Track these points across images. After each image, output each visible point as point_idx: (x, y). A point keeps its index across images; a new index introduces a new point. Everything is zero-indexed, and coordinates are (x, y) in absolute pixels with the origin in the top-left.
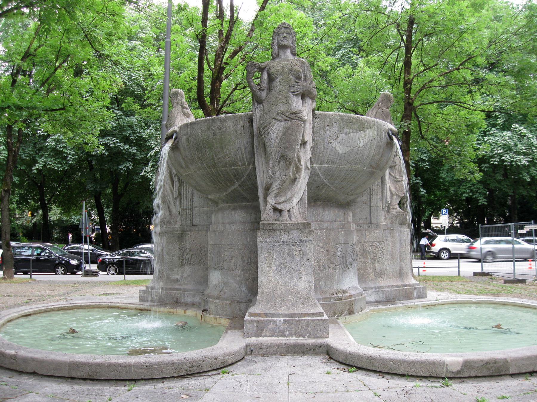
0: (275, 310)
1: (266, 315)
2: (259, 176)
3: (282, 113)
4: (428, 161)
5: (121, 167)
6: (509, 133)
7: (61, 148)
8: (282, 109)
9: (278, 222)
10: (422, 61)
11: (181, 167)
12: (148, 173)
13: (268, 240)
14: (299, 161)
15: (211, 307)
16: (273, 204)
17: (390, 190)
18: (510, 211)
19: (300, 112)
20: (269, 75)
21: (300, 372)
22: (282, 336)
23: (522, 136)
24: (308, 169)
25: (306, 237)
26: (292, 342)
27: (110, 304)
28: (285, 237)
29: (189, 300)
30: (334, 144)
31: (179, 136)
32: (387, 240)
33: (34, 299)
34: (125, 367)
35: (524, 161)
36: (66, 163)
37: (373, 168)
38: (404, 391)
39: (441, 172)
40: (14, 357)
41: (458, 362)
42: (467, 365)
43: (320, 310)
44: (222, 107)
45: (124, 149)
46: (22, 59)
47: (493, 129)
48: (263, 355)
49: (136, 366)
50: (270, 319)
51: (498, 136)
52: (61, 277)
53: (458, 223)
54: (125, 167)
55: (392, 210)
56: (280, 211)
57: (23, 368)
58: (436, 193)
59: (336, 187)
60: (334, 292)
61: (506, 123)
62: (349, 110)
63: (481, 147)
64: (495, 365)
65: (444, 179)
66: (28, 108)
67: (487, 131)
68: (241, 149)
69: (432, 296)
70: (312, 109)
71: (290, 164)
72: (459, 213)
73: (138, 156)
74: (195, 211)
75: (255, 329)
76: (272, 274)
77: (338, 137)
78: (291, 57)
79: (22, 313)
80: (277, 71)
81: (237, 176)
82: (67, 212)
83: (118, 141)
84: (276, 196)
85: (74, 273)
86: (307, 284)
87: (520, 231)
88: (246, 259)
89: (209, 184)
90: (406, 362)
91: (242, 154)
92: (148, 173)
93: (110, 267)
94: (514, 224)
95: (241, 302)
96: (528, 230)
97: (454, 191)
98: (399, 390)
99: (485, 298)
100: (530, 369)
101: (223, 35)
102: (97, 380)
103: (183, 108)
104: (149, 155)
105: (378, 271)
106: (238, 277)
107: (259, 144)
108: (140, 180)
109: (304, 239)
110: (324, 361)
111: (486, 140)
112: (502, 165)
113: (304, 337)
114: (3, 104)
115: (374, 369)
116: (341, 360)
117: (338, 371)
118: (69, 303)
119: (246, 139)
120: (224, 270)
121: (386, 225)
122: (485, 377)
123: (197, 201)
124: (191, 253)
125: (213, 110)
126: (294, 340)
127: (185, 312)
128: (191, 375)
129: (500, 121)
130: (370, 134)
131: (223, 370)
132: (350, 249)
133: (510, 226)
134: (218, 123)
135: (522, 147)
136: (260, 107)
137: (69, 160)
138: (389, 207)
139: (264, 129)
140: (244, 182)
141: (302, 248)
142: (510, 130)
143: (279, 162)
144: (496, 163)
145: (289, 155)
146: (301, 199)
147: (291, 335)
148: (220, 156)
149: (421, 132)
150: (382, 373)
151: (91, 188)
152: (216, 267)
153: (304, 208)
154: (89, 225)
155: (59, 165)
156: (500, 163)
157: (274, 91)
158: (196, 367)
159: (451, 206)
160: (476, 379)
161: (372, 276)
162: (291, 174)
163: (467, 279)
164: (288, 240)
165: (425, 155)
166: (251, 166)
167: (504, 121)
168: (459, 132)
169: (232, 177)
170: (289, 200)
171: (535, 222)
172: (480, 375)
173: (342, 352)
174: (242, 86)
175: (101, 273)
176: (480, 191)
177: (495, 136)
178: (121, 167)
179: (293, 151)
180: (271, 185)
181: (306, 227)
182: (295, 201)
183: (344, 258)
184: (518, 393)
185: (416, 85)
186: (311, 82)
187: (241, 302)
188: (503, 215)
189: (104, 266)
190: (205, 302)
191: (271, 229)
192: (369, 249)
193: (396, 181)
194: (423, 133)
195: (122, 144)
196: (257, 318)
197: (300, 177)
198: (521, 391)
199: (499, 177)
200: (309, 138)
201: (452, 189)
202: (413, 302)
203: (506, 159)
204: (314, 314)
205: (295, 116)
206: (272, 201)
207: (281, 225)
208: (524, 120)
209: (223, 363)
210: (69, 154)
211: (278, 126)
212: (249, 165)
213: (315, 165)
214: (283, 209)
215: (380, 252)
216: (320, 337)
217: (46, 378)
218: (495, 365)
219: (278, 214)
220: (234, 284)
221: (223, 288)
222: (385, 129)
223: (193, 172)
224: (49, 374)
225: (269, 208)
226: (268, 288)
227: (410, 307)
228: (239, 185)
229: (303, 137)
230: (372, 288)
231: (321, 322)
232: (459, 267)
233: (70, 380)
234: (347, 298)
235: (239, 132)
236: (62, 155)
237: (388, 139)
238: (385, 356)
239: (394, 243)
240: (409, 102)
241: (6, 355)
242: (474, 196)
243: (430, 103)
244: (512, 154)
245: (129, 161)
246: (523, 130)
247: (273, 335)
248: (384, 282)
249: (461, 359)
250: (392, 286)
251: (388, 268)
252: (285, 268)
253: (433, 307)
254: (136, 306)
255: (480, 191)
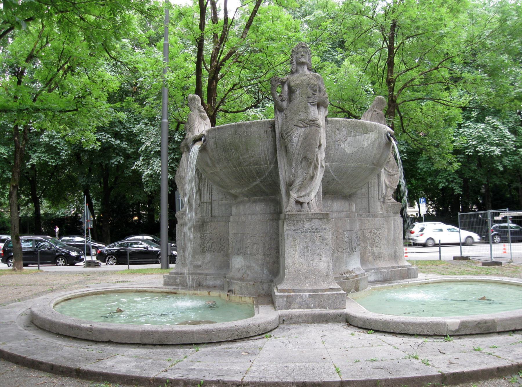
0: (301, 286)
1: (294, 291)
2: (282, 174)
3: (302, 121)
4: (406, 152)
5: (112, 161)
6: (483, 126)
7: (54, 143)
8: (302, 117)
9: (300, 213)
10: (402, 60)
11: (208, 165)
12: (140, 167)
13: (293, 228)
14: (318, 161)
15: (236, 287)
16: (295, 197)
17: (385, 183)
18: (483, 199)
19: (317, 120)
20: (290, 88)
21: (328, 335)
22: (308, 308)
23: (495, 128)
24: (323, 167)
25: (325, 225)
26: (317, 312)
27: (137, 289)
28: (307, 226)
29: (211, 283)
30: (343, 146)
31: (207, 139)
32: (383, 227)
33: (55, 287)
34: (188, 333)
35: (497, 151)
36: (60, 158)
37: (374, 165)
38: (416, 345)
39: (419, 162)
40: (90, 330)
41: (456, 323)
42: (463, 325)
43: (337, 286)
44: (219, 105)
45: (116, 144)
46: (27, 61)
47: (468, 121)
48: (293, 324)
49: (198, 332)
50: (297, 294)
51: (472, 129)
52: (62, 268)
53: (433, 211)
54: (116, 161)
55: (387, 201)
56: (301, 204)
57: (99, 338)
58: (412, 182)
59: (343, 182)
60: (342, 272)
61: (480, 115)
62: (336, 106)
63: (457, 138)
64: (485, 325)
65: (421, 169)
66: (44, 110)
67: (462, 124)
68: (264, 151)
69: (422, 277)
70: (325, 116)
71: (311, 164)
72: (433, 201)
73: (129, 151)
74: (215, 204)
75: (285, 303)
76: (297, 257)
77: (346, 140)
78: (308, 72)
79: (65, 297)
80: (297, 85)
81: (259, 173)
82: (55, 206)
83: (109, 136)
84: (298, 191)
85: (73, 264)
86: (326, 264)
87: (496, 218)
88: (267, 245)
89: (233, 180)
90: (415, 324)
91: (265, 155)
92: (140, 167)
93: (109, 258)
94: (490, 211)
95: (264, 283)
96: (503, 216)
97: (431, 180)
98: (412, 345)
99: (469, 277)
100: (513, 328)
101: (217, 37)
102: (165, 345)
103: (200, 111)
104: (140, 150)
105: (376, 254)
106: (260, 261)
107: (281, 147)
108: (131, 174)
109: (323, 226)
110: (345, 327)
111: (461, 132)
112: (477, 155)
113: (326, 308)
114: (21, 106)
115: (389, 331)
116: (359, 326)
117: (360, 333)
118: (85, 290)
119: (269, 142)
120: (246, 255)
121: (383, 214)
122: (477, 334)
123: (216, 195)
124: (212, 241)
125: (210, 109)
126: (317, 311)
127: (209, 293)
128: (241, 339)
129: (474, 114)
130: (373, 136)
131: (267, 334)
132: (354, 235)
133: (486, 213)
134: (244, 128)
135: (495, 139)
136: (281, 115)
137: (62, 155)
138: (384, 198)
139: (286, 134)
140: (265, 178)
141: (322, 234)
142: (483, 123)
143: (301, 162)
144: (471, 154)
145: (310, 156)
146: (317, 193)
147: (315, 307)
148: (245, 157)
149: (403, 127)
150: (395, 334)
151: (82, 182)
152: (239, 252)
153: (320, 200)
154: (90, 218)
155: (53, 161)
156: (475, 154)
157: (295, 102)
158: (244, 333)
159: (426, 194)
160: (470, 336)
161: (371, 259)
162: (311, 172)
163: (447, 263)
164: (310, 228)
165: (404, 147)
166: (272, 165)
167: (478, 114)
168: (438, 126)
169: (255, 174)
170: (308, 194)
171: (509, 210)
172: (473, 333)
173: (360, 319)
174: (238, 86)
175: (103, 264)
176: (455, 181)
177: (469, 128)
178: (112, 161)
179: (313, 152)
180: (293, 181)
181: (325, 217)
182: (313, 195)
183: (350, 243)
184: (505, 344)
185: (399, 85)
186: (325, 94)
187: (264, 283)
188: (476, 203)
189: (103, 257)
190: (229, 284)
191: (295, 219)
192: (368, 235)
193: (391, 175)
194: (405, 128)
195: (113, 140)
196: (286, 294)
197: (317, 174)
198: (507, 343)
199: (474, 167)
200: (323, 141)
201: (430, 179)
202: (407, 282)
203: (480, 150)
204: (333, 289)
205: (312, 123)
206: (294, 195)
207: (303, 215)
208: (497, 113)
209: (265, 329)
210: (62, 150)
211: (299, 131)
212: (271, 164)
213: (327, 164)
214: (304, 201)
215: (377, 238)
216: (339, 308)
217: (120, 345)
218: (485, 325)
219: (299, 206)
220: (256, 267)
221: (246, 271)
222: (385, 131)
223: (219, 170)
224: (124, 342)
225: (292, 201)
226: (294, 268)
227: (404, 286)
228: (261, 182)
229: (320, 141)
230: (371, 270)
231: (340, 296)
232: (440, 252)
233: (141, 346)
234: (354, 277)
235: (262, 136)
236: (56, 150)
237: (387, 140)
238: (398, 320)
239: (389, 230)
240: (392, 99)
241: (81, 328)
242: (450, 186)
243: (412, 100)
244: (485, 145)
245: (121, 156)
246: (496, 122)
247: (300, 308)
248: (381, 264)
249: (458, 321)
250: (389, 268)
251: (384, 252)
252: (308, 251)
253: (424, 285)
254: (162, 290)
255: (455, 181)
